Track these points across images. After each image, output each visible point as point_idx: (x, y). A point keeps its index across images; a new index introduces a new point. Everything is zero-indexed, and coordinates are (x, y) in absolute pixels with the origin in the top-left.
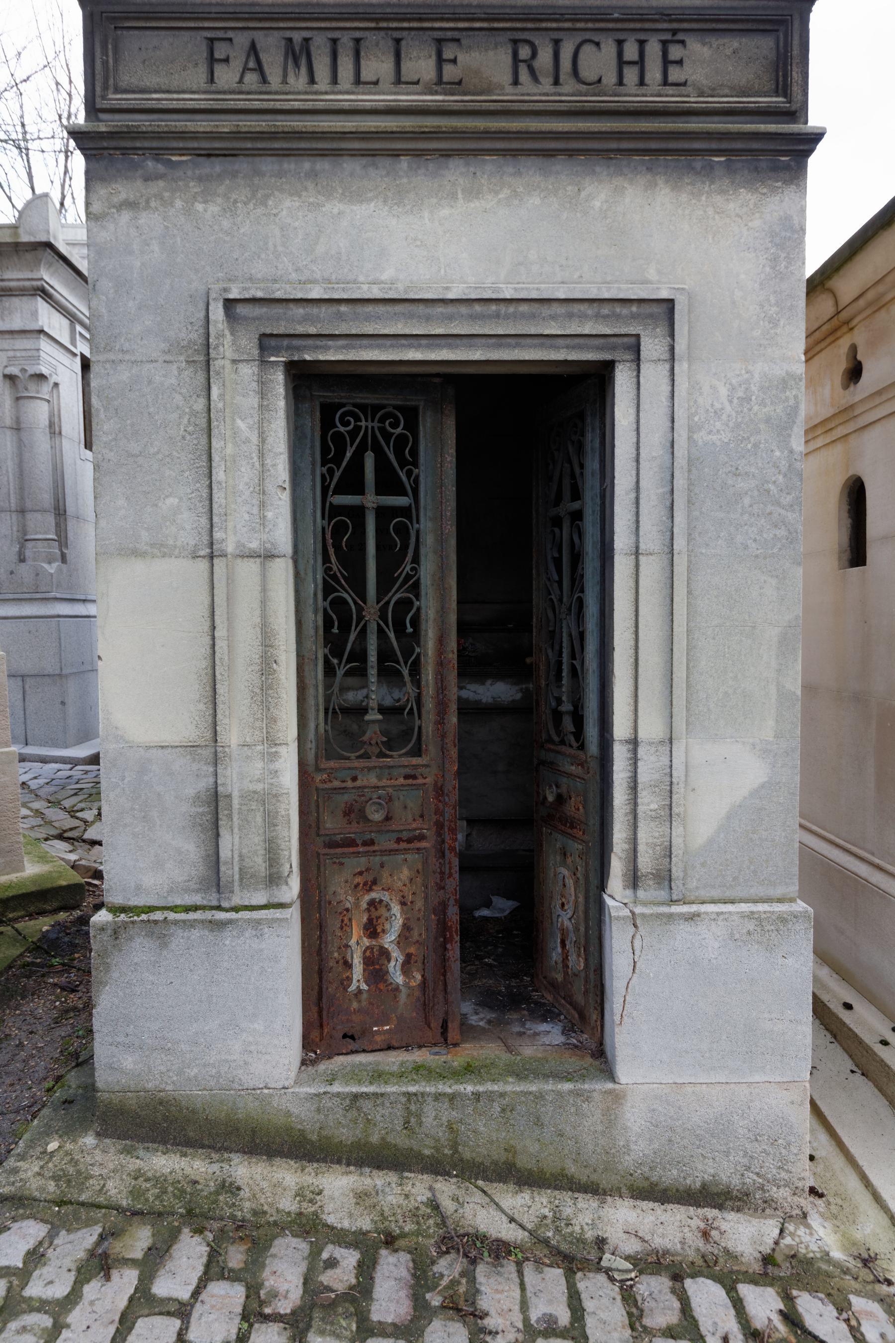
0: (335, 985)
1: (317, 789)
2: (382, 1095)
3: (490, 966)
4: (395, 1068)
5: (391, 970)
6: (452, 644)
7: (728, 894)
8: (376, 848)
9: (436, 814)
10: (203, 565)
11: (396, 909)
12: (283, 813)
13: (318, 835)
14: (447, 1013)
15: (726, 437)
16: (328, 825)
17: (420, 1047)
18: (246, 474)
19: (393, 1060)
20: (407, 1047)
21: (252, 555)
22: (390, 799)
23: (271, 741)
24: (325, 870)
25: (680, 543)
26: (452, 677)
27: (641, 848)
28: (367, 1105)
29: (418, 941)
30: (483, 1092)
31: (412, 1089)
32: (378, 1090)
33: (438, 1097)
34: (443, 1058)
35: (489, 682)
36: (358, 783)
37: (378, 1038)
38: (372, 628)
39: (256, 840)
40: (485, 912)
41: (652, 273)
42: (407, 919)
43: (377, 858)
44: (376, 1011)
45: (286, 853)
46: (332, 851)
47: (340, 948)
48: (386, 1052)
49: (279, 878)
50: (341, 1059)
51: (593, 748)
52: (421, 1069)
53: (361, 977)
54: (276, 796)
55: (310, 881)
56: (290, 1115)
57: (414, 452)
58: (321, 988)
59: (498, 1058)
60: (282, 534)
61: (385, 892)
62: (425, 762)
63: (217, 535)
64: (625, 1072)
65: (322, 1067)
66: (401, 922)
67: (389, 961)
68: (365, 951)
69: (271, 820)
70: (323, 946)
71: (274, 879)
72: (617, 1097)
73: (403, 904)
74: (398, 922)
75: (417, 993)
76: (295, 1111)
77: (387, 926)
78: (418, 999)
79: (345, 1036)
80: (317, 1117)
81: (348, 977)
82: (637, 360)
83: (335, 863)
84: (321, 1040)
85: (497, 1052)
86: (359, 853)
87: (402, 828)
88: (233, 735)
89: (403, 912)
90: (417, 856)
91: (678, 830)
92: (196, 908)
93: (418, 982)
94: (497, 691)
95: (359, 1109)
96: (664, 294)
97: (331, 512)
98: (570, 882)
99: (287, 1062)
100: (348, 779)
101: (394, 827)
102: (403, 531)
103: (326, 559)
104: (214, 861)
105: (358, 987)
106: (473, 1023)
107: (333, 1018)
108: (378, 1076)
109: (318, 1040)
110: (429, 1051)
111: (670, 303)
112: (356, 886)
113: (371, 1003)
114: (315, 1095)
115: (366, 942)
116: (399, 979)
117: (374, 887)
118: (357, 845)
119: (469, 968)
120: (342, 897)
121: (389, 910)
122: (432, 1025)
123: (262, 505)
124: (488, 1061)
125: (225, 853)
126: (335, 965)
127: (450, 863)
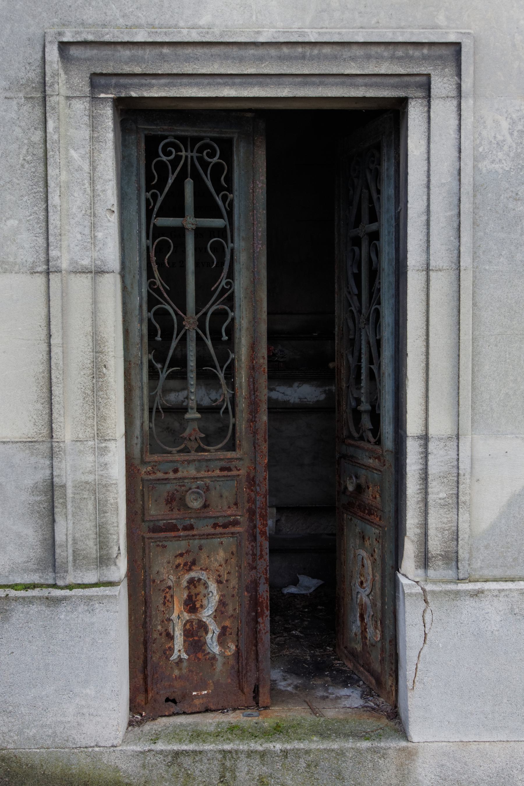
0: (158, 655)
2: (201, 752)
3: (297, 637)
4: (212, 729)
5: (209, 641)
6: (263, 351)
7: (509, 573)
8: (195, 532)
10: (40, 280)
11: (213, 587)
12: (112, 501)
13: (143, 521)
14: (258, 679)
15: (507, 165)
16: (152, 512)
17: (234, 710)
18: (79, 199)
19: (210, 721)
20: (222, 710)
21: (84, 271)
22: (208, 489)
23: (101, 436)
24: (150, 552)
25: (466, 261)
26: (263, 380)
27: (431, 532)
28: (187, 761)
29: (232, 616)
30: (290, 750)
31: (227, 747)
32: (197, 748)
33: (250, 754)
34: (255, 720)
35: (296, 384)
36: (179, 475)
38: (192, 336)
39: (88, 526)
40: (293, 590)
41: (441, 19)
45: (115, 537)
47: (163, 621)
49: (109, 559)
50: (164, 720)
51: (388, 442)
52: (236, 729)
54: (105, 486)
56: (119, 771)
57: (229, 179)
58: (146, 657)
59: (304, 719)
60: (110, 252)
61: (203, 572)
62: (238, 456)
63: (53, 253)
64: (416, 732)
65: (147, 727)
66: (217, 598)
67: (207, 633)
68: (185, 625)
69: (101, 507)
70: (148, 620)
71: (104, 560)
72: (410, 755)
73: (219, 582)
74: (214, 599)
75: (232, 662)
76: (123, 766)
77: (205, 602)
78: (233, 667)
79: (167, 700)
81: (170, 648)
82: (428, 97)
83: (158, 546)
84: (146, 704)
85: (303, 714)
86: (180, 537)
87: (218, 514)
88: (67, 432)
89: (219, 589)
90: (231, 539)
91: (464, 517)
92: (34, 586)
94: (304, 392)
95: (180, 765)
96: (452, 38)
97: (155, 233)
98: (368, 563)
99: (115, 723)
102: (219, 249)
103: (150, 275)
104: (51, 544)
105: (179, 656)
108: (197, 735)
109: (143, 703)
110: (243, 713)
111: (457, 46)
112: (178, 566)
113: (190, 671)
114: (141, 752)
115: (186, 616)
116: (216, 649)
117: (193, 567)
118: (178, 530)
120: (165, 576)
121: (206, 588)
122: (245, 690)
123: (93, 226)
125: (60, 537)
126: (158, 637)
127: (261, 546)
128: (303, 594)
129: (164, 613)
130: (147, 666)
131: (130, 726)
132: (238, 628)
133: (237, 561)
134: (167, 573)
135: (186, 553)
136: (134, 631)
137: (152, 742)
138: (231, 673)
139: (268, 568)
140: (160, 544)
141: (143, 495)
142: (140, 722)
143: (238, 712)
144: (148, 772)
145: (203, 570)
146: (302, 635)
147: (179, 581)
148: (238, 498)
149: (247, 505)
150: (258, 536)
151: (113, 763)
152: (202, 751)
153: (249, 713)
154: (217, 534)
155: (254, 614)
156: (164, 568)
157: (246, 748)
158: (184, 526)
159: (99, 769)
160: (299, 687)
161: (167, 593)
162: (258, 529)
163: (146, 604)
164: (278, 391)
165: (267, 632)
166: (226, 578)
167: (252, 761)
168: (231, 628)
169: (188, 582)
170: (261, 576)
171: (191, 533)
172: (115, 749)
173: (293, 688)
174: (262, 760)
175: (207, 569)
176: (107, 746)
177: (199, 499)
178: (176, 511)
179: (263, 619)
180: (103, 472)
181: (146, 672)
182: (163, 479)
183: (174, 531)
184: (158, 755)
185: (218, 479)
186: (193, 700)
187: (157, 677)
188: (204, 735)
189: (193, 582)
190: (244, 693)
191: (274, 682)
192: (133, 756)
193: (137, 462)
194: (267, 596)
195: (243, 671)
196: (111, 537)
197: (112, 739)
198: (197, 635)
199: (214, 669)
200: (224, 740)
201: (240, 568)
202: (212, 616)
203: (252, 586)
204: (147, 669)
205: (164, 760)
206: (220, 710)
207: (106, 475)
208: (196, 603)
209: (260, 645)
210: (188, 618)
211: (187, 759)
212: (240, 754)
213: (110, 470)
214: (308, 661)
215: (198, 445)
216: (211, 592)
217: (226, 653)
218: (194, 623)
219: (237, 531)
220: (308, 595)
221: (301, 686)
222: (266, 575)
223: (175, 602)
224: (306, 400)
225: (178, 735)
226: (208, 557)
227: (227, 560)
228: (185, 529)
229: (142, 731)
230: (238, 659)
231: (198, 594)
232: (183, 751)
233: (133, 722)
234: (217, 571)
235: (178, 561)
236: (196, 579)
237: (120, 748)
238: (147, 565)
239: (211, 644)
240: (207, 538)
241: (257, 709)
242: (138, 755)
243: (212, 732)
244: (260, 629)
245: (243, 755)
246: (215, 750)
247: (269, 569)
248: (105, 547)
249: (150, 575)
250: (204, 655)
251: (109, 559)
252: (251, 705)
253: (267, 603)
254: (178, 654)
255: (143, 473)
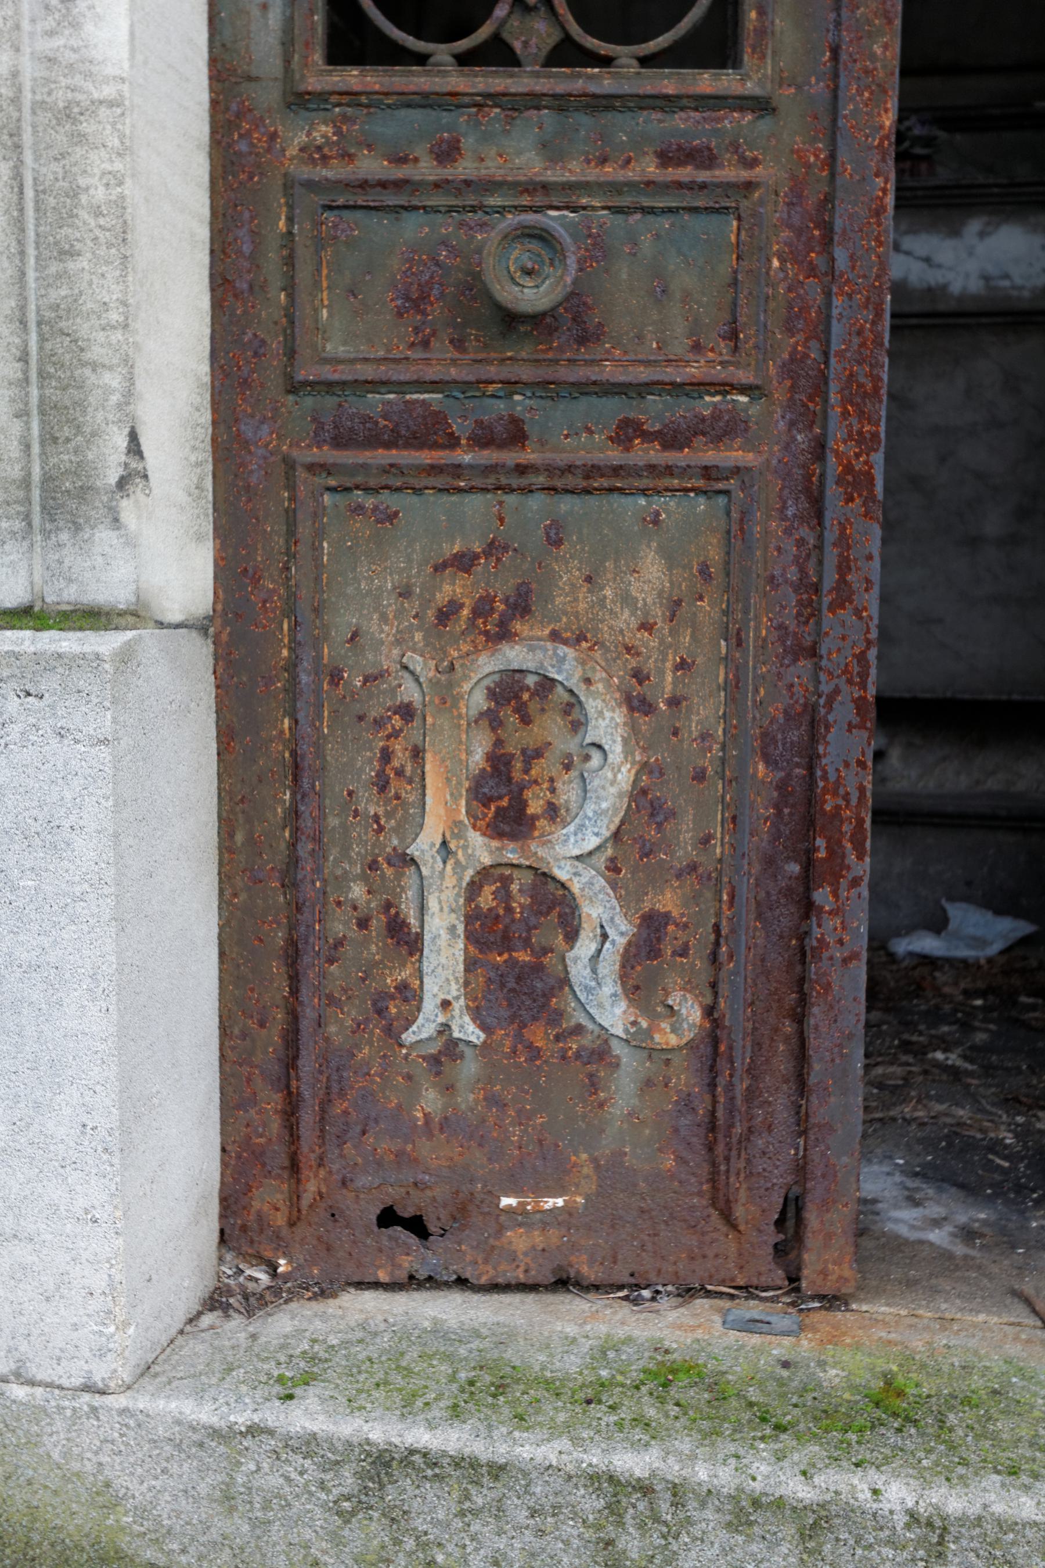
0: (349, 1015)
1: (289, 185)
2: (498, 1470)
3: (955, 1073)
4: (572, 1364)
5: (579, 972)
8: (530, 456)
9: (790, 331)
11: (606, 721)
12: (100, 194)
13: (294, 388)
14: (801, 1169)
16: (334, 348)
17: (687, 1293)
19: (571, 1330)
20: (632, 1288)
24: (319, 534)
28: (431, 1506)
29: (693, 868)
30: (962, 1520)
31: (632, 1462)
32: (480, 1449)
33: (746, 1512)
34: (780, 1347)
35: (974, 226)
36: (465, 168)
37: (518, 1240)
40: (928, 944)
42: (644, 767)
43: (536, 502)
44: (515, 1134)
45: (113, 380)
46: (348, 457)
47: (373, 865)
48: (549, 1298)
49: (84, 493)
50: (370, 1301)
52: (683, 1380)
53: (454, 990)
54: (68, 115)
55: (256, 580)
56: (113, 1505)
58: (294, 1017)
59: (1021, 1372)
61: (563, 650)
62: (750, 87)
65: (290, 1324)
66: (625, 777)
67: (572, 936)
68: (474, 889)
70: (305, 848)
71: (62, 499)
73: (638, 705)
75: (684, 1078)
76: (131, 1483)
77: (568, 793)
78: (687, 1104)
79: (388, 1218)
80: (221, 1525)
81: (403, 987)
83: (359, 509)
84: (292, 1224)
85: (1013, 1350)
86: (457, 470)
87: (643, 374)
89: (633, 736)
90: (702, 504)
93: (689, 1036)
95: (396, 1518)
99: (99, 1282)
100: (421, 150)
101: (609, 372)
105: (445, 1028)
106: (904, 1231)
107: (341, 1140)
108: (495, 1387)
109: (280, 1220)
110: (724, 1313)
112: (446, 615)
113: (492, 1100)
114: (215, 1433)
115: (481, 849)
116: (610, 1012)
117: (517, 626)
118: (453, 442)
119: (879, 1070)
120: (388, 658)
121: (577, 726)
122: (739, 1212)
124: (976, 1381)
126: (353, 932)
127: (843, 541)
128: (964, 961)
129: (381, 829)
130: (296, 1057)
131: (212, 1309)
132: (717, 928)
133: (726, 613)
134: (398, 642)
135: (488, 553)
136: (243, 896)
137: (277, 1389)
138: (676, 1130)
139: (872, 654)
140: (369, 502)
141: (290, 261)
142: (262, 1297)
143: (701, 1303)
144: (246, 1528)
145: (565, 642)
146: (969, 1067)
147: (450, 685)
148: (742, 301)
149: (786, 344)
150: (832, 491)
151: (89, 1467)
152: (502, 1468)
153: (755, 1314)
154: (634, 471)
155: (794, 868)
156: (384, 618)
157: (725, 1478)
158: (479, 423)
159: (30, 1483)
160: (982, 1236)
161: (395, 734)
162: (832, 459)
163: (296, 779)
164: (908, 253)
165: (854, 956)
166: (668, 688)
167: (754, 1547)
168: (686, 926)
169: (492, 694)
170: (837, 691)
171: (511, 457)
172: (98, 1400)
173: (953, 1235)
174: (811, 1553)
175: (581, 638)
176: (65, 1382)
177: (547, 270)
178: (442, 349)
179: (835, 894)
180: (59, 42)
181: (294, 1083)
182: (383, 185)
183: (435, 446)
184: (292, 1456)
185: (646, 202)
186: (501, 1230)
187: (345, 1113)
188: (536, 1390)
189: (518, 697)
190: (734, 1227)
191: (868, 1204)
192: (179, 1446)
193: (267, 96)
194: (862, 789)
195: (732, 1126)
196: (92, 378)
197: (88, 1354)
198: (527, 943)
199: (601, 1105)
200: (620, 1425)
201: (739, 644)
202: (601, 860)
203: (794, 736)
204: (295, 1067)
205: (322, 1486)
206: (621, 1288)
207: (71, 57)
208: (528, 794)
209: (816, 1013)
210: (487, 860)
211: (430, 1496)
212: (692, 1505)
213: (89, 28)
214: (1006, 1147)
215: (556, 37)
216: (599, 747)
217: (657, 1037)
218: (515, 887)
219: (731, 464)
220: (983, 962)
221: (986, 1230)
222: (863, 686)
223: (429, 781)
224: (1006, 283)
225: (408, 1372)
226: (589, 579)
227: (678, 603)
228: (483, 439)
229: (254, 1337)
230: (712, 1068)
231: (538, 754)
232: (412, 1452)
233: (230, 1293)
234: (628, 649)
235: (447, 588)
236: (531, 680)
237: (120, 1401)
238: (303, 592)
239: (588, 990)
240: (587, 491)
241: (793, 1304)
242: (201, 1445)
243: (566, 1378)
244: (821, 941)
245: (709, 1514)
246: (570, 1468)
247: (879, 658)
248: (67, 432)
249: (317, 644)
250: (558, 1038)
251: (84, 493)
252: (764, 1280)
253: (861, 822)
254: (441, 1019)
255: (292, 151)
